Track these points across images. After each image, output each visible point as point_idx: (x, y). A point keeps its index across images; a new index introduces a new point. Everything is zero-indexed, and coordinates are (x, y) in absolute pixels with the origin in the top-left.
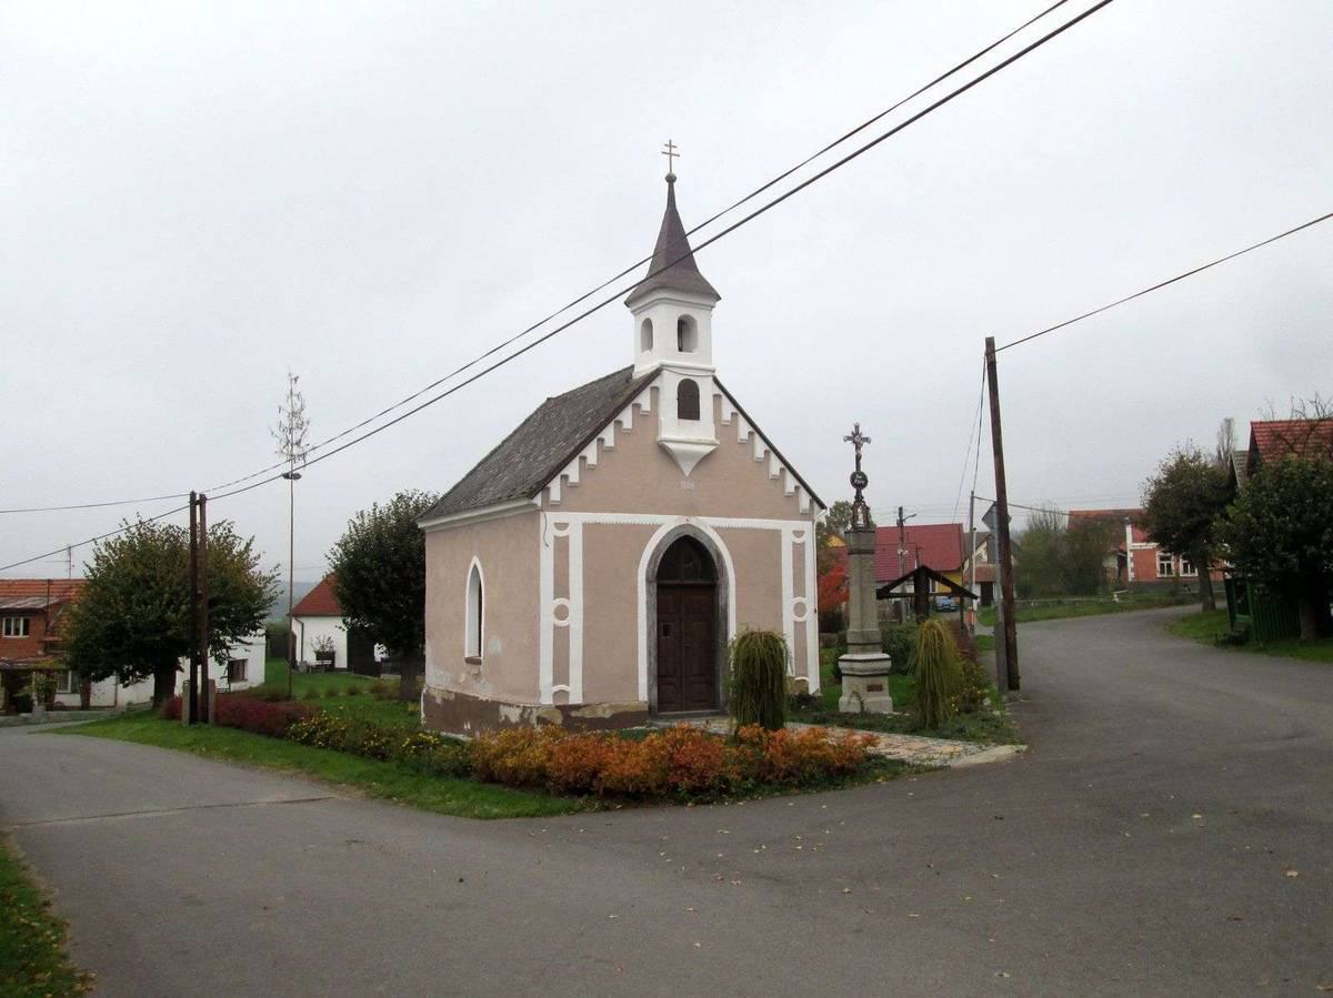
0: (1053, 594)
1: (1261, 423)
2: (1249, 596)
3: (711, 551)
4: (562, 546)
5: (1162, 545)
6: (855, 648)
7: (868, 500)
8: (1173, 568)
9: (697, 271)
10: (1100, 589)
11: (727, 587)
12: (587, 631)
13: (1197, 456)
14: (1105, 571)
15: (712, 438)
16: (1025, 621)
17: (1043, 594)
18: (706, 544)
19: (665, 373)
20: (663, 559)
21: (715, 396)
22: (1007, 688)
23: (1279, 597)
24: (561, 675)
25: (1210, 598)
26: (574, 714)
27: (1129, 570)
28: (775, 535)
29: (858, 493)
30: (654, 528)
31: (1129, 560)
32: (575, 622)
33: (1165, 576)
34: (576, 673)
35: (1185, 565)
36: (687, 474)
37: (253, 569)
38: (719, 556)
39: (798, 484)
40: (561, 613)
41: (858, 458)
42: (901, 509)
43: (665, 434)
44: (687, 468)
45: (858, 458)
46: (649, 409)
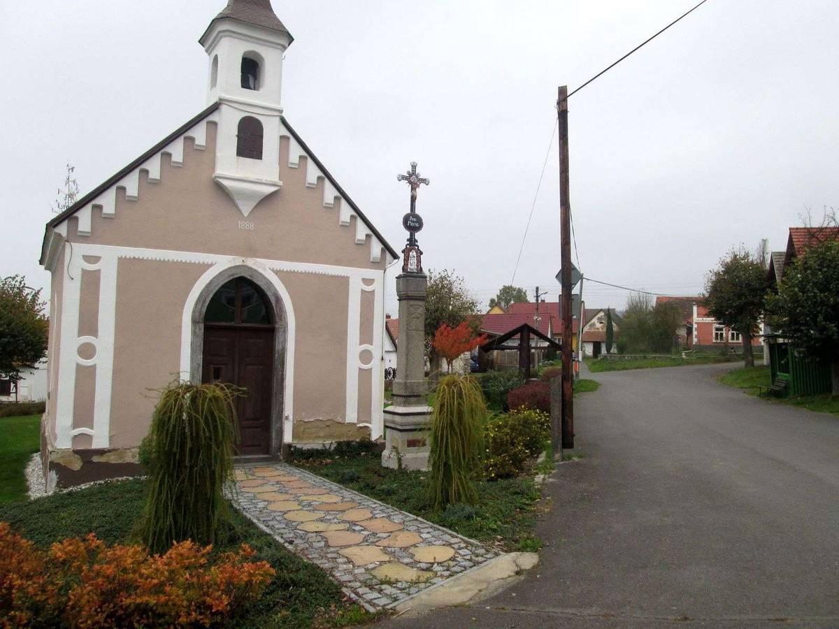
0: (641, 351)
1: (797, 229)
2: (790, 359)
3: (269, 294)
4: (91, 282)
5: (718, 318)
6: (400, 399)
7: (421, 244)
8: (724, 335)
9: (271, 10)
10: (673, 350)
11: (285, 331)
12: (116, 372)
13: (747, 256)
14: (678, 337)
15: (276, 179)
16: (619, 370)
17: (634, 351)
18: (264, 287)
19: (224, 108)
20: (212, 299)
21: (282, 137)
22: (560, 446)
23: (818, 359)
24: (83, 414)
25: (750, 358)
26: (96, 459)
27: (694, 336)
28: (344, 282)
29: (412, 235)
30: (206, 267)
31: (694, 329)
32: (104, 362)
33: (719, 341)
34: (102, 413)
35: (733, 334)
36: (246, 215)
37: (41, 313)
38: (278, 299)
39: (369, 232)
40: (87, 351)
41: (413, 199)
42: (537, 288)
43: (220, 171)
44: (246, 208)
45: (413, 199)
46: (204, 143)
